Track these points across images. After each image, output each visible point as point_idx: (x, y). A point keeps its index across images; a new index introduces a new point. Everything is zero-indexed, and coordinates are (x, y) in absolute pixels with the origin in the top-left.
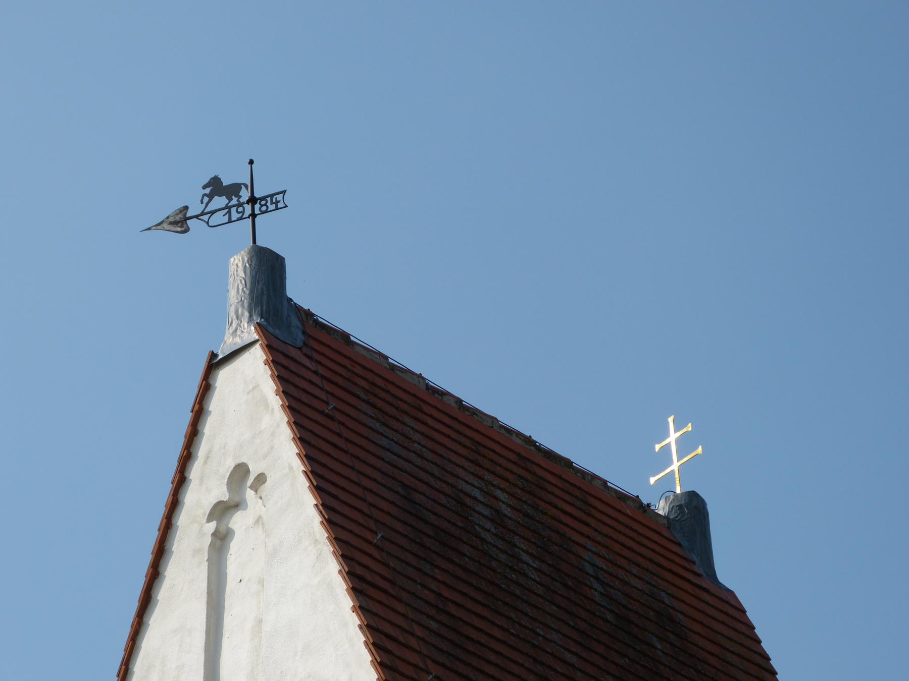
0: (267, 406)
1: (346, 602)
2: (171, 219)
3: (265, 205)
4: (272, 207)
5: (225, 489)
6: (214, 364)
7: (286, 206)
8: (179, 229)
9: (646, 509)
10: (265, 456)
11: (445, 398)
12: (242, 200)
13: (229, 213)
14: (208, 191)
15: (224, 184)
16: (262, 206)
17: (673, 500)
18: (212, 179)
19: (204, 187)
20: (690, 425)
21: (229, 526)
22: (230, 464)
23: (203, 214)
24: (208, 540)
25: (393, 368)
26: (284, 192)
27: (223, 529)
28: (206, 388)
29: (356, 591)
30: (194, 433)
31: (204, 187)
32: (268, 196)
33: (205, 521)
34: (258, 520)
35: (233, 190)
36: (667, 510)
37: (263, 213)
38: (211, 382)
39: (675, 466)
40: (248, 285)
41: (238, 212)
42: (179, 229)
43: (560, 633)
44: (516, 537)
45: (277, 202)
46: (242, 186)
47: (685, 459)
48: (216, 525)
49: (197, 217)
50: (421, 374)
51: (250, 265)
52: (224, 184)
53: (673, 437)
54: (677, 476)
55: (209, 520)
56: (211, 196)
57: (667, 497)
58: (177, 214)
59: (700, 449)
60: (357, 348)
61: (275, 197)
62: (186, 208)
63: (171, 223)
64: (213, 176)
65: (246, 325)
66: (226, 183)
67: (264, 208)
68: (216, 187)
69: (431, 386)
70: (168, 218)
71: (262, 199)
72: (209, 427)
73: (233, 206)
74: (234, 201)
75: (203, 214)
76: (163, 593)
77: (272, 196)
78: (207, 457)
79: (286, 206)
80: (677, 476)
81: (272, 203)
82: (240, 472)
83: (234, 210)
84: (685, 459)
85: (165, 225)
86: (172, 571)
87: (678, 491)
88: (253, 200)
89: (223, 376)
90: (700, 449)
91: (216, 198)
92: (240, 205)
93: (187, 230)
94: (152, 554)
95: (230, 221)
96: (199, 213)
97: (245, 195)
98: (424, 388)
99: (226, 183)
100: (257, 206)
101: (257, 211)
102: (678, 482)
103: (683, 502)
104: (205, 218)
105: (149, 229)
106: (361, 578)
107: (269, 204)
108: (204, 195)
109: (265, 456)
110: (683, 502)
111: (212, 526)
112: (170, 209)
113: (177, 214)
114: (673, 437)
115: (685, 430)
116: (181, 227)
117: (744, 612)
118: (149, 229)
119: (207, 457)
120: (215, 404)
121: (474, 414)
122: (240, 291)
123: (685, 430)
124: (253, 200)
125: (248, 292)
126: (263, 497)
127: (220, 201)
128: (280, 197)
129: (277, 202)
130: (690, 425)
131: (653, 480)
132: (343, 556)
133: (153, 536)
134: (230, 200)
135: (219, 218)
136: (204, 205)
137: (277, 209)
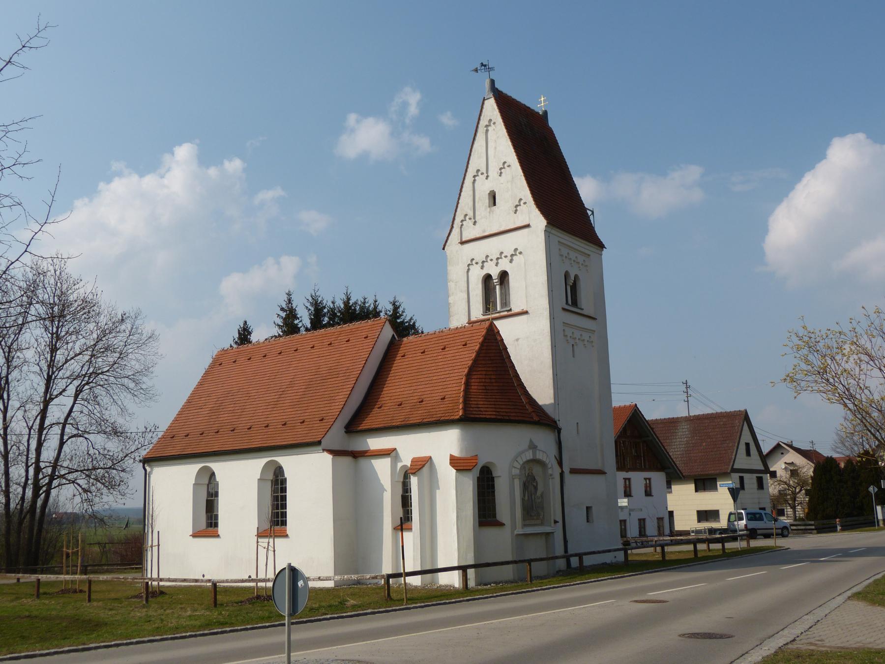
6: (484, 100)
9: (538, 113)
28: (483, 103)
29: (515, 148)
34: (494, 129)
35: (485, 66)
39: (543, 104)
43: (70, 384)
44: (441, 575)
46: (571, 304)
50: (561, 429)
53: (542, 99)
68: (482, 65)
76: (477, 138)
88: (489, 68)
89: (486, 102)
97: (487, 67)
99: (484, 64)
106: (518, 153)
111: (485, 129)
114: (542, 99)
120: (485, 106)
127: (483, 67)
133: (475, 128)
135: (483, 71)
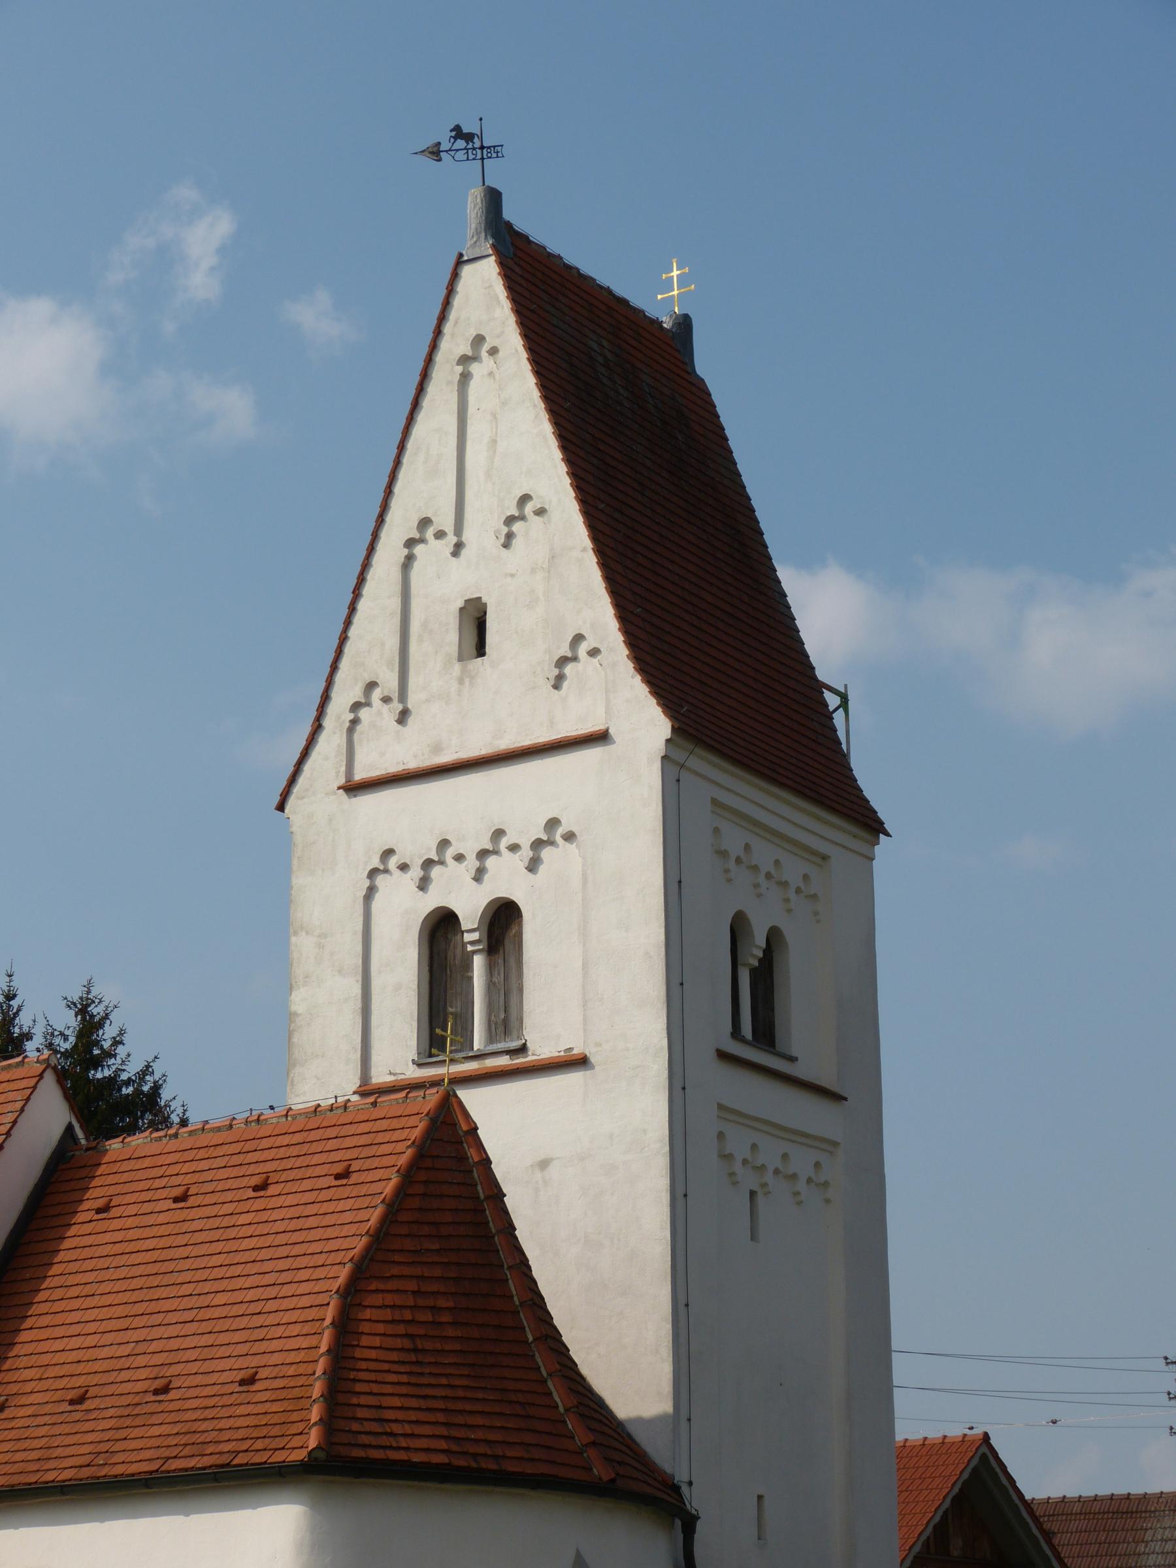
0: (499, 302)
1: (558, 455)
2: (430, 150)
3: (488, 153)
4: (494, 155)
5: (469, 347)
6: (460, 262)
7: (503, 156)
8: (436, 158)
9: (657, 323)
10: (498, 337)
11: (573, 271)
12: (475, 146)
13: (467, 152)
14: (453, 134)
15: (464, 132)
16: (488, 153)
17: (675, 318)
18: (456, 126)
19: (451, 131)
20: (687, 268)
21: (470, 369)
22: (473, 333)
23: (450, 150)
24: (458, 377)
25: (550, 255)
26: (502, 146)
27: (466, 372)
28: (455, 275)
30: (447, 303)
31: (451, 131)
32: (492, 147)
33: (455, 364)
34: (491, 374)
35: (469, 137)
36: (671, 323)
37: (489, 158)
38: (458, 272)
39: (675, 292)
40: (484, 212)
41: (473, 154)
42: (436, 158)
45: (498, 152)
47: (683, 290)
48: (462, 370)
49: (446, 151)
51: (485, 199)
52: (464, 132)
53: (675, 273)
54: (676, 299)
55: (459, 363)
56: (455, 138)
57: (671, 315)
58: (434, 147)
59: (693, 286)
60: (533, 246)
61: (496, 148)
62: (439, 144)
63: (430, 153)
64: (456, 124)
65: (483, 241)
66: (465, 131)
67: (489, 155)
68: (459, 133)
69: (567, 264)
70: (428, 148)
71: (489, 148)
72: (457, 302)
73: (469, 149)
74: (470, 146)
75: (450, 150)
76: (426, 402)
77: (494, 147)
78: (456, 323)
79: (503, 156)
80: (676, 299)
81: (494, 152)
82: (479, 340)
83: (470, 151)
84: (683, 290)
85: (426, 153)
86: (432, 389)
87: (676, 311)
88: (482, 148)
89: (467, 271)
90: (693, 286)
91: (459, 141)
92: (474, 149)
93: (440, 160)
94: (420, 375)
95: (468, 159)
96: (448, 149)
97: (477, 144)
98: (562, 264)
99: (465, 131)
100: (485, 151)
101: (485, 156)
102: (676, 304)
103: (681, 321)
104: (452, 153)
105: (416, 153)
107: (492, 152)
108: (451, 137)
109: (498, 337)
110: (681, 321)
111: (460, 369)
112: (430, 142)
113: (434, 147)
114: (675, 273)
115: (684, 271)
116: (437, 157)
117: (710, 395)
118: (416, 153)
119: (456, 323)
120: (461, 287)
121: (586, 279)
122: (479, 216)
123: (684, 271)
124: (482, 148)
125: (484, 218)
126: (497, 362)
127: (461, 143)
128: (499, 149)
129: (498, 152)
130: (687, 268)
131: (659, 297)
132: (555, 423)
134: (468, 144)
135: (461, 155)
136: (451, 144)
137: (497, 157)
